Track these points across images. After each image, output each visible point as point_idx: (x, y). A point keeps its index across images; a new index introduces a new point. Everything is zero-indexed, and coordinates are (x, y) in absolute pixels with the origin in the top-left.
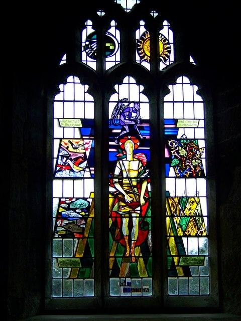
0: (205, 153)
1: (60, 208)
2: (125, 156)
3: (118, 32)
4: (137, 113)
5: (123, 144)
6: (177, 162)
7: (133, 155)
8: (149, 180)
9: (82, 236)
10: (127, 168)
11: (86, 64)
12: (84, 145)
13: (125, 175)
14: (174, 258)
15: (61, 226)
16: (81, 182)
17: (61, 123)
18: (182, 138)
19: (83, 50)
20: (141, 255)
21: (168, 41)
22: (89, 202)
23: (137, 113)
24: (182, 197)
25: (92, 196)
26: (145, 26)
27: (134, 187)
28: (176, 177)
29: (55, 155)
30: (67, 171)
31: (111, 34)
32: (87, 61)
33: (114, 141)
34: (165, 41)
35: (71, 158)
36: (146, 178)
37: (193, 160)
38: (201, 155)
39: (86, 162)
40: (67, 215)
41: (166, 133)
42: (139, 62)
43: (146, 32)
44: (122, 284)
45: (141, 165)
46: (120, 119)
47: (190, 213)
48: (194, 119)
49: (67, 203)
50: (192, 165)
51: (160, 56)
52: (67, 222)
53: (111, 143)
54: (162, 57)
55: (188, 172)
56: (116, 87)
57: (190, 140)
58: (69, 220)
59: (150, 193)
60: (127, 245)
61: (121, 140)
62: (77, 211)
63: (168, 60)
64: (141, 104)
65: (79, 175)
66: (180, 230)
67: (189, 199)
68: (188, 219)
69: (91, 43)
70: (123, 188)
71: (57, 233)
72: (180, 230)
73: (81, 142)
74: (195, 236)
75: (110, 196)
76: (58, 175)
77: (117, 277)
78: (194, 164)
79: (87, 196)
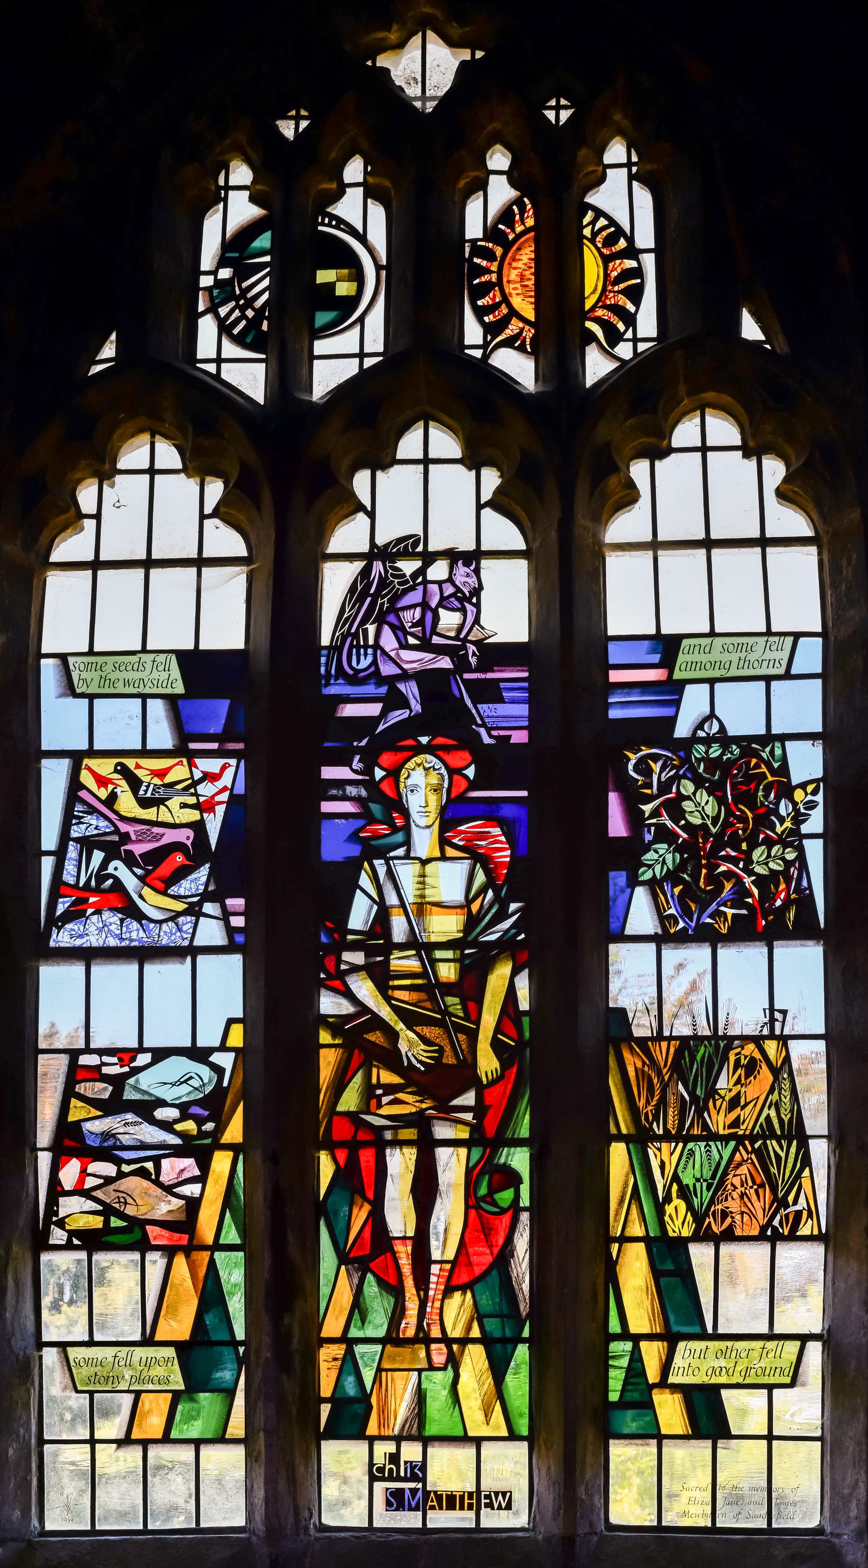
0: (820, 809)
1: (74, 1102)
2: (399, 837)
3: (377, 213)
4: (464, 611)
5: (394, 774)
6: (669, 858)
7: (442, 831)
8: (524, 956)
9: (184, 1240)
10: (410, 897)
11: (217, 377)
12: (195, 784)
13: (399, 929)
14: (644, 1345)
15: (80, 1191)
16: (180, 970)
17: (75, 676)
18: (701, 734)
19: (201, 308)
20: (476, 1333)
21: (630, 240)
22: (219, 1070)
23: (464, 611)
24: (695, 1037)
25: (236, 1038)
26: (513, 176)
27: (448, 988)
28: (660, 940)
29: (49, 839)
30: (112, 918)
31: (340, 223)
32: (219, 360)
33: (349, 764)
34: (610, 241)
35: (129, 853)
36: (505, 946)
37: (753, 846)
38: (799, 818)
39: (203, 872)
40: (107, 1135)
41: (614, 714)
42: (478, 353)
43: (518, 202)
44: (381, 1470)
45: (480, 878)
46: (377, 646)
47: (736, 1123)
48: (769, 633)
49: (106, 1079)
50: (750, 873)
51: (585, 315)
52: (108, 1169)
53: (329, 773)
54: (598, 321)
55: (730, 912)
56: (361, 482)
57: (746, 742)
58: (118, 1162)
59: (526, 1020)
60: (409, 1283)
61: (387, 759)
62: (161, 1114)
63: (629, 335)
64: (484, 563)
65: (167, 936)
66: (677, 1209)
67: (729, 1048)
68: (726, 1154)
69: (243, 271)
70: (388, 999)
71: (61, 1224)
72: (677, 1209)
73: (179, 772)
74: (761, 1237)
75: (325, 1037)
76: (62, 938)
77: (360, 1434)
78: (760, 870)
79: (208, 1038)
